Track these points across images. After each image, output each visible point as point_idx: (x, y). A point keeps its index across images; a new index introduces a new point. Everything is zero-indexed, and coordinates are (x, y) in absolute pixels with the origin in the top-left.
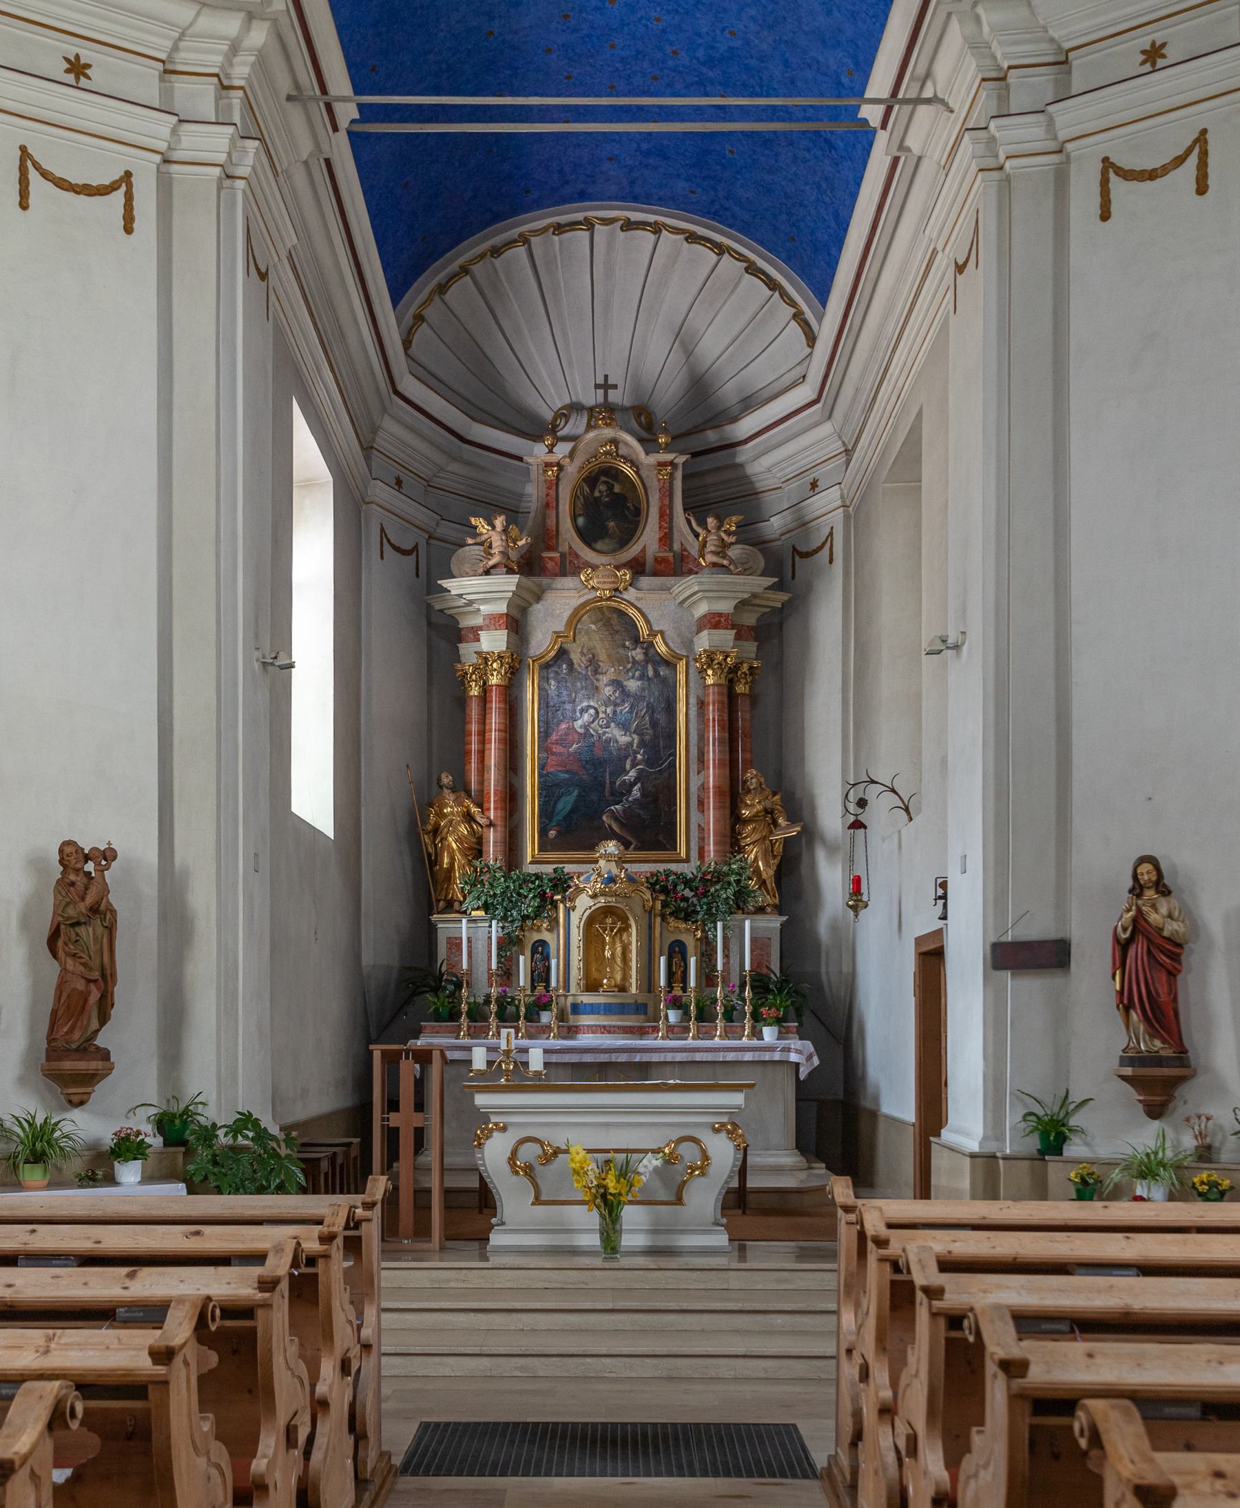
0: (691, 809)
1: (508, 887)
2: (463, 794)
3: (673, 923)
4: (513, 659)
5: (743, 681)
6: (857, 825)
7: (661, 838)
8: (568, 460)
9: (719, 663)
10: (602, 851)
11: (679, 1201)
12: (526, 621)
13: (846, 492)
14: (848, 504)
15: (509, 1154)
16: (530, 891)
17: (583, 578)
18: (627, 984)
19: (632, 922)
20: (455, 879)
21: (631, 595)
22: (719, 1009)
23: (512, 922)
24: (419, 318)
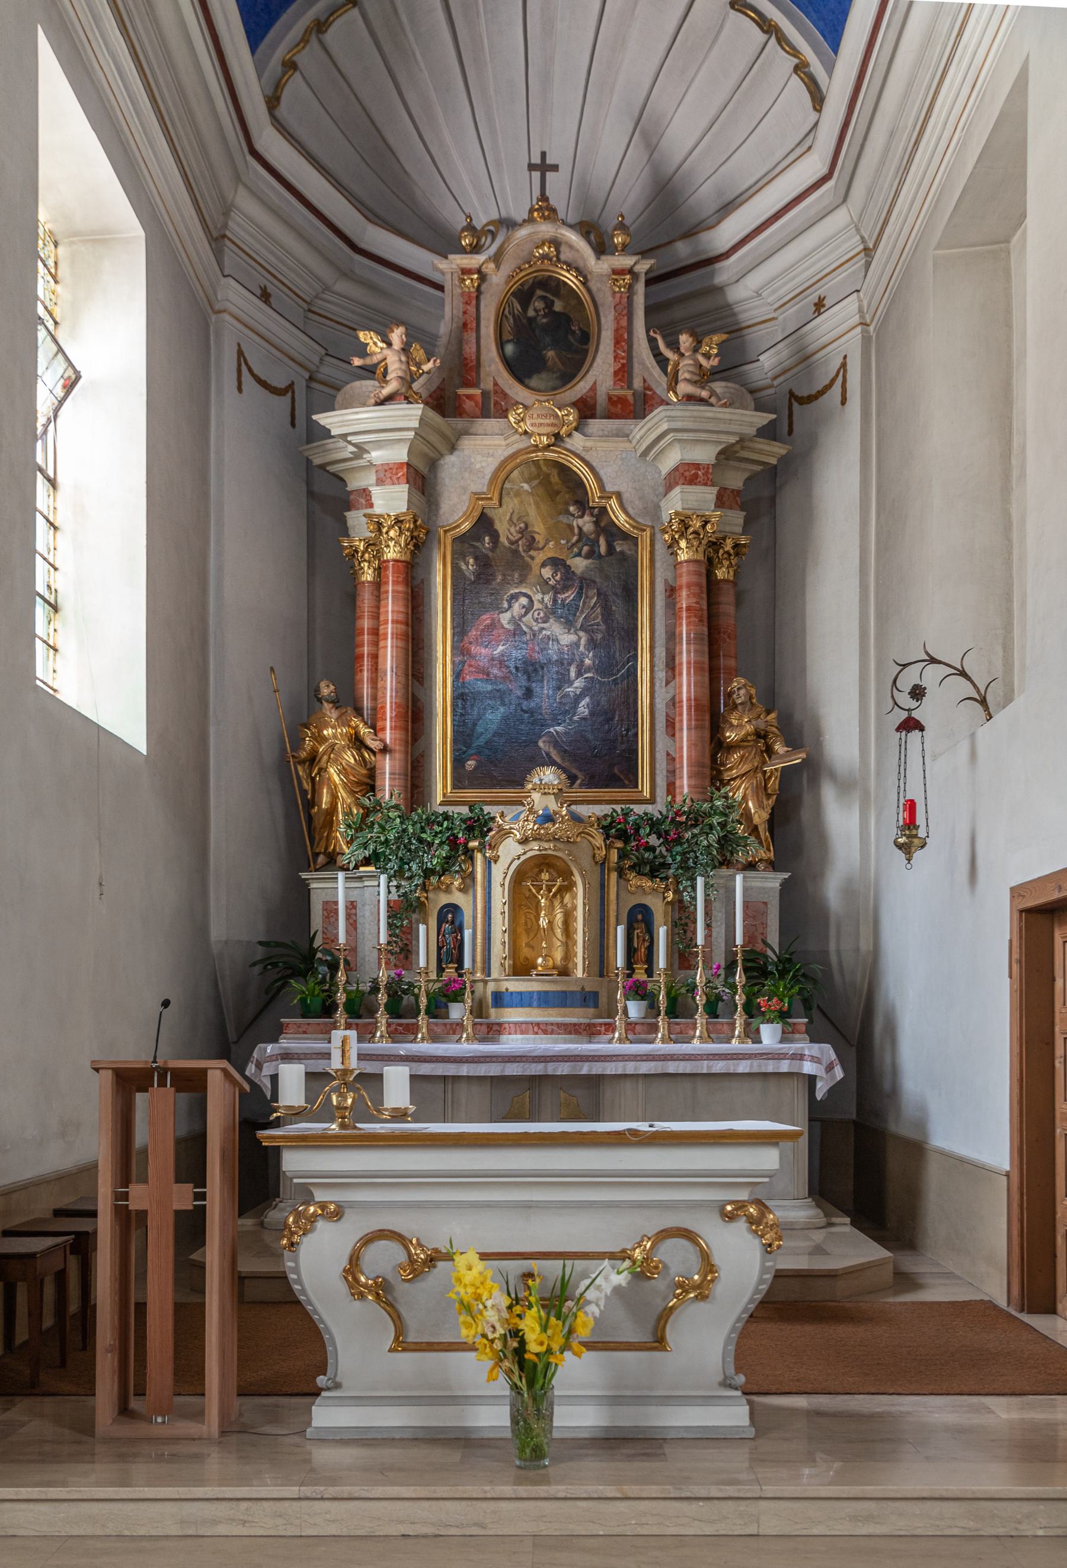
0: (658, 732)
1: (405, 831)
2: (350, 710)
3: (635, 880)
4: (416, 527)
5: (726, 563)
6: (911, 725)
7: (616, 770)
8: (492, 266)
9: (695, 532)
10: (536, 780)
11: (659, 1342)
12: (436, 477)
13: (865, 303)
14: (868, 321)
15: (344, 1263)
16: (435, 836)
17: (512, 420)
18: (570, 965)
19: (578, 879)
20: (338, 824)
21: (577, 442)
22: (700, 999)
23: (410, 878)
24: (290, 66)
